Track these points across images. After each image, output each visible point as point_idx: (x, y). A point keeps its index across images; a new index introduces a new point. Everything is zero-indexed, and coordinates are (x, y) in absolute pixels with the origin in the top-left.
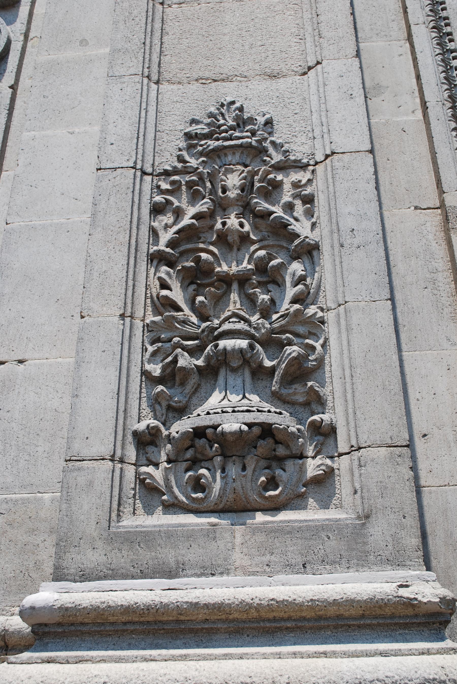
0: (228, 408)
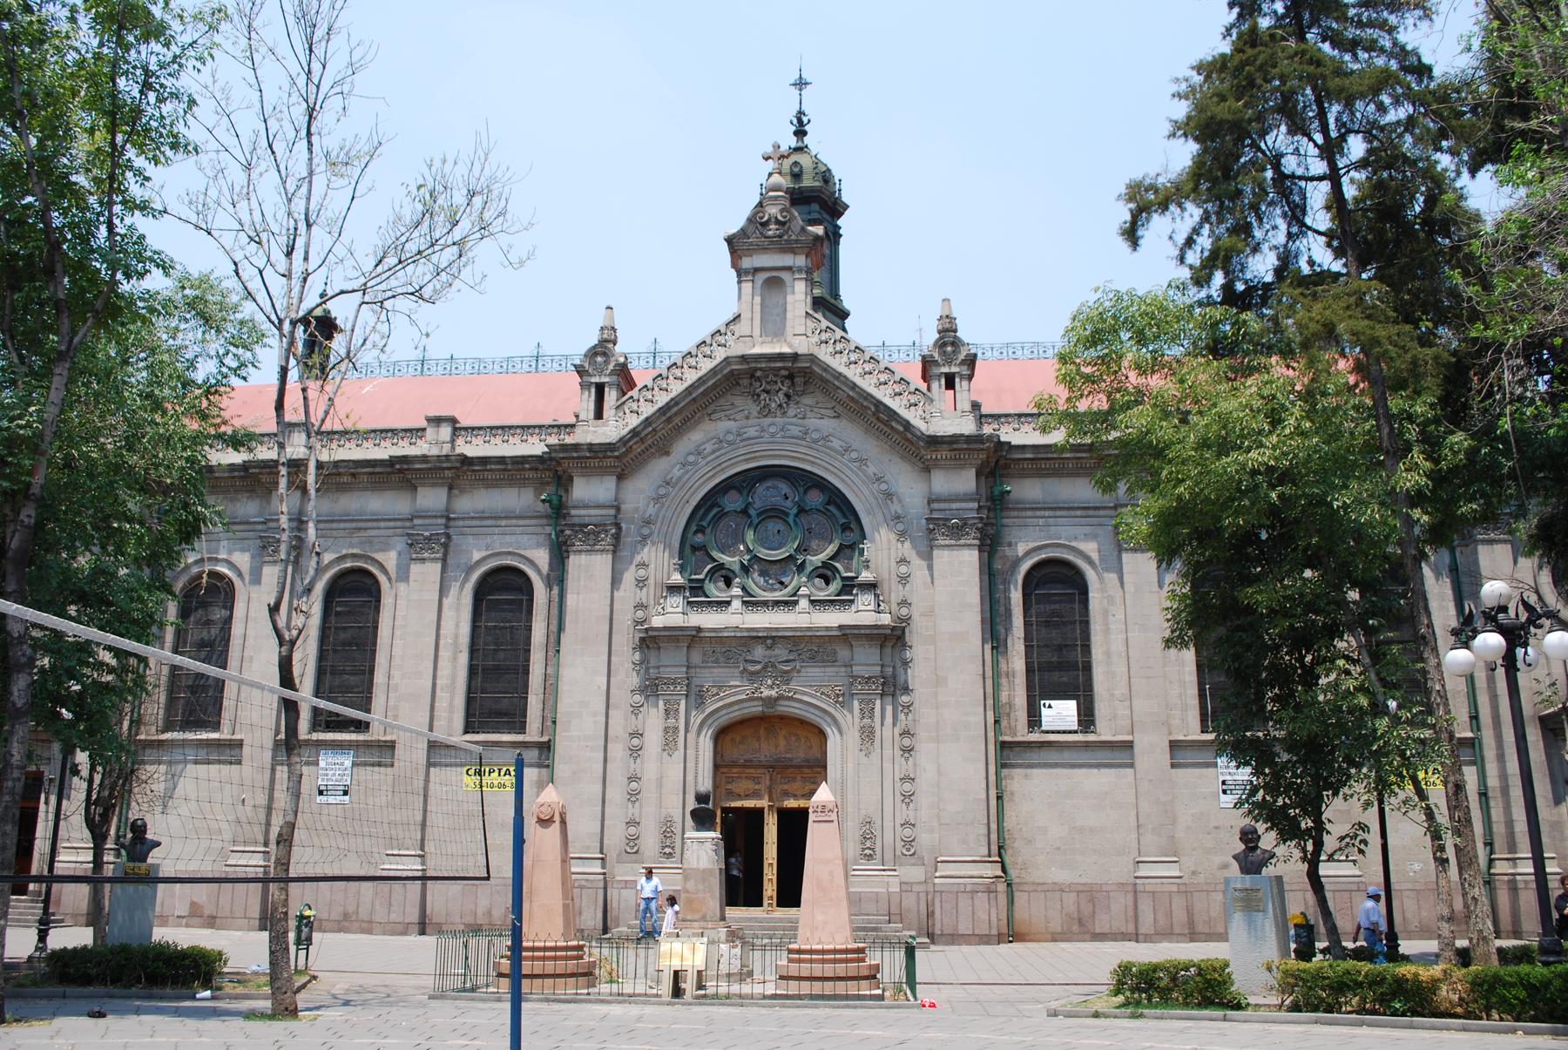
0: (667, 850)
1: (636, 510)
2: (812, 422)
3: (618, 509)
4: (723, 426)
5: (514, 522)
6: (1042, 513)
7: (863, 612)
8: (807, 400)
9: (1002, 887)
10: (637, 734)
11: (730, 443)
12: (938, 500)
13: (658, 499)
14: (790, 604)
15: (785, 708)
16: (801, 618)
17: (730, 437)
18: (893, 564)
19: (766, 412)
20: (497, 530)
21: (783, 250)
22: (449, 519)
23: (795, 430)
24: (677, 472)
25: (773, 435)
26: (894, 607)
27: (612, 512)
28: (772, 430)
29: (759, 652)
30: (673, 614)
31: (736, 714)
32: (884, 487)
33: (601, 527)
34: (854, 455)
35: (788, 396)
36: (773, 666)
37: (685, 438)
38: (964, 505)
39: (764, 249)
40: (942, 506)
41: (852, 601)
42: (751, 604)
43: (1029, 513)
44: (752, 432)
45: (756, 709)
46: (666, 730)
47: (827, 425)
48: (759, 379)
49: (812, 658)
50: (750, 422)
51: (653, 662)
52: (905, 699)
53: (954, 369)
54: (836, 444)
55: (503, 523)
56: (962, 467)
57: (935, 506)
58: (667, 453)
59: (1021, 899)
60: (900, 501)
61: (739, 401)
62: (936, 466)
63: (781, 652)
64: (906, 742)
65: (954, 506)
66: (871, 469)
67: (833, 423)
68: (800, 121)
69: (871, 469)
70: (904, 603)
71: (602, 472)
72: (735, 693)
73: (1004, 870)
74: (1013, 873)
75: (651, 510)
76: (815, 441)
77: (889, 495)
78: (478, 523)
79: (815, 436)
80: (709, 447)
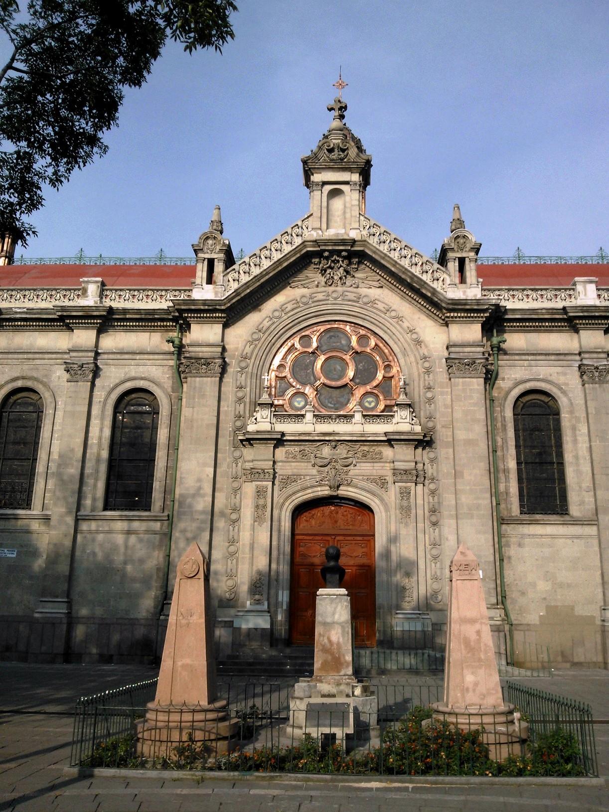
1: (237, 349)
2: (363, 291)
3: (224, 349)
5: (146, 356)
6: (527, 357)
11: (305, 304)
12: (455, 346)
14: (348, 417)
15: (344, 491)
17: (304, 300)
18: (422, 391)
19: (330, 283)
20: (133, 362)
21: (344, 169)
22: (97, 354)
23: (351, 296)
24: (266, 324)
25: (336, 299)
26: (423, 420)
28: (334, 295)
29: (326, 451)
31: (309, 495)
32: (414, 336)
34: (393, 314)
37: (272, 300)
38: (473, 349)
40: (457, 349)
41: (393, 416)
43: (517, 357)
44: (320, 296)
45: (324, 491)
46: (257, 506)
50: (319, 289)
52: (432, 486)
53: (464, 255)
54: (380, 306)
55: (138, 357)
56: (472, 322)
58: (260, 311)
59: (518, 636)
60: (426, 346)
62: (453, 322)
63: (342, 451)
64: (434, 519)
67: (379, 291)
70: (430, 418)
71: (213, 320)
74: (513, 617)
75: (248, 350)
76: (366, 304)
77: (419, 342)
78: (119, 356)
79: (365, 300)
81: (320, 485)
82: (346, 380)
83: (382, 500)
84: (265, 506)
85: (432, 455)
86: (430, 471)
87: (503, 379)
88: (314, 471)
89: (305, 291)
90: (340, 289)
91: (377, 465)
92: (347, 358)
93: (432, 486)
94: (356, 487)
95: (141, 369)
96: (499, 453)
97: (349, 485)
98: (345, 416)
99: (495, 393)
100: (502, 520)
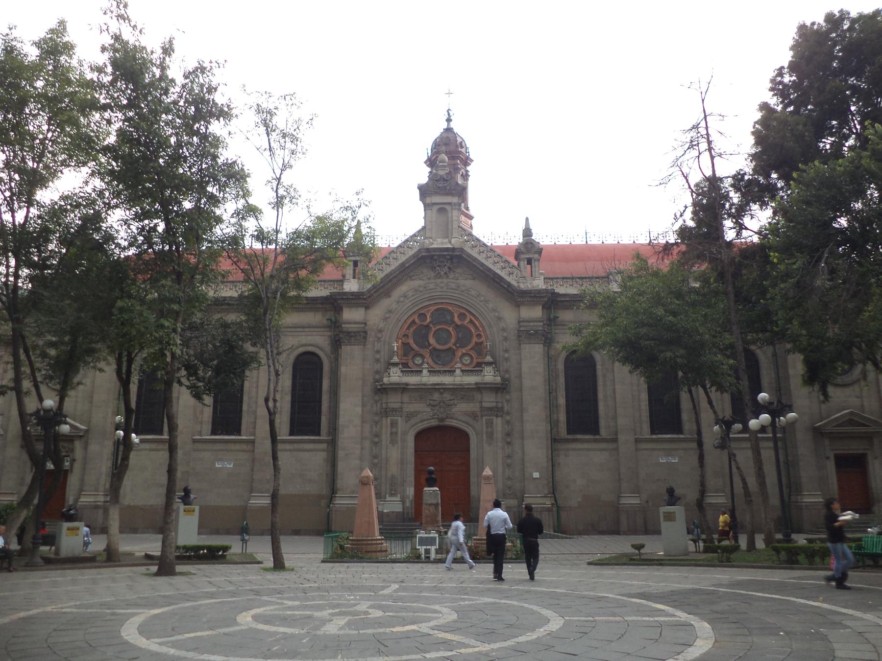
2: (461, 282)
4: (417, 283)
7: (489, 376)
8: (459, 270)
9: (555, 509)
10: (377, 435)
13: (385, 319)
14: (451, 372)
16: (459, 379)
19: (438, 276)
23: (453, 286)
27: (363, 326)
29: (436, 396)
30: (395, 376)
32: (497, 314)
33: (356, 333)
34: (482, 298)
35: (449, 268)
36: (444, 402)
39: (436, 193)
42: (432, 372)
44: (432, 286)
45: (434, 423)
46: (391, 433)
47: (469, 283)
48: (435, 260)
49: (462, 398)
51: (384, 401)
52: (508, 418)
54: (473, 293)
57: (522, 324)
58: (390, 297)
59: (563, 515)
61: (425, 271)
65: (531, 324)
66: (491, 306)
68: (449, 114)
69: (491, 306)
71: (358, 306)
72: (425, 415)
73: (556, 501)
74: (560, 502)
75: (382, 325)
77: (500, 319)
79: (463, 288)
80: (410, 294)
81: (433, 418)
82: (450, 345)
83: (474, 428)
84: (396, 433)
85: (508, 397)
86: (506, 408)
87: (558, 342)
88: (428, 409)
89: (421, 282)
90: (445, 280)
91: (471, 405)
92: (451, 329)
93: (508, 418)
94: (456, 419)
95: (309, 338)
96: (554, 394)
97: (451, 418)
98: (449, 371)
99: (552, 353)
100: (555, 440)
